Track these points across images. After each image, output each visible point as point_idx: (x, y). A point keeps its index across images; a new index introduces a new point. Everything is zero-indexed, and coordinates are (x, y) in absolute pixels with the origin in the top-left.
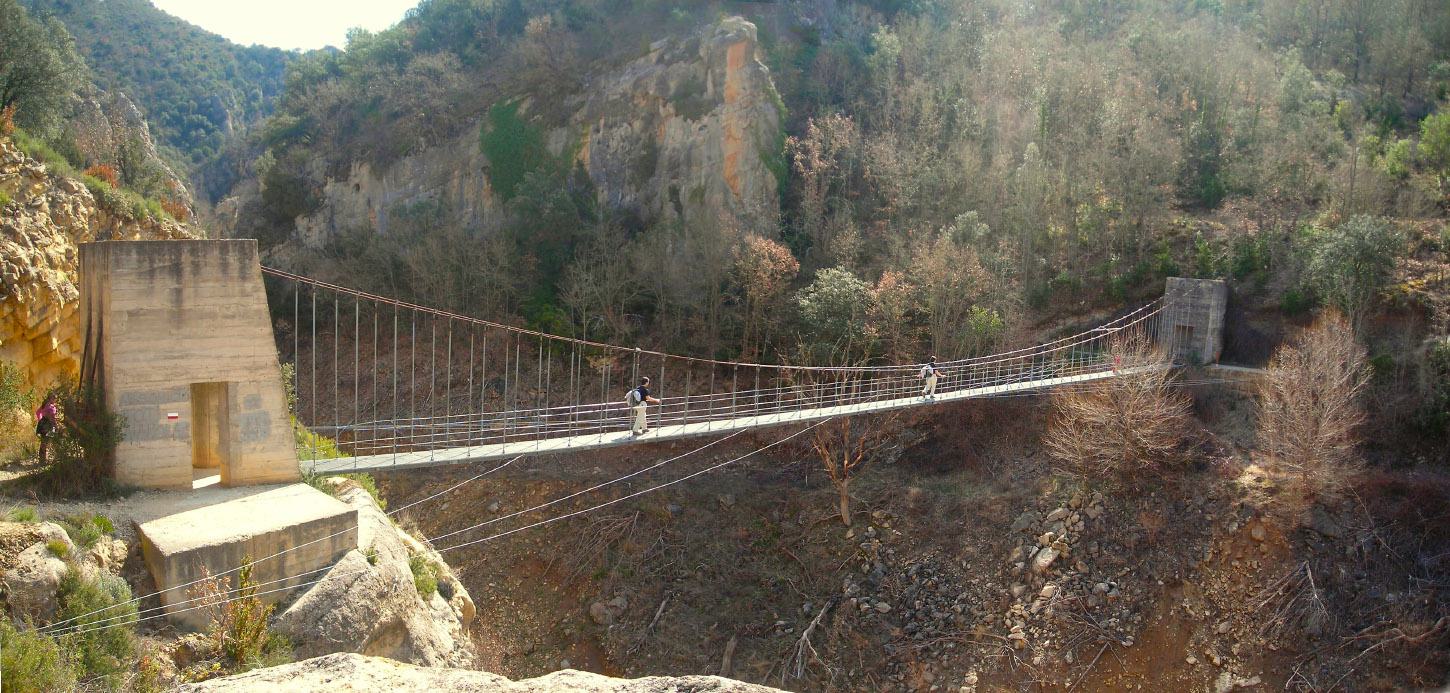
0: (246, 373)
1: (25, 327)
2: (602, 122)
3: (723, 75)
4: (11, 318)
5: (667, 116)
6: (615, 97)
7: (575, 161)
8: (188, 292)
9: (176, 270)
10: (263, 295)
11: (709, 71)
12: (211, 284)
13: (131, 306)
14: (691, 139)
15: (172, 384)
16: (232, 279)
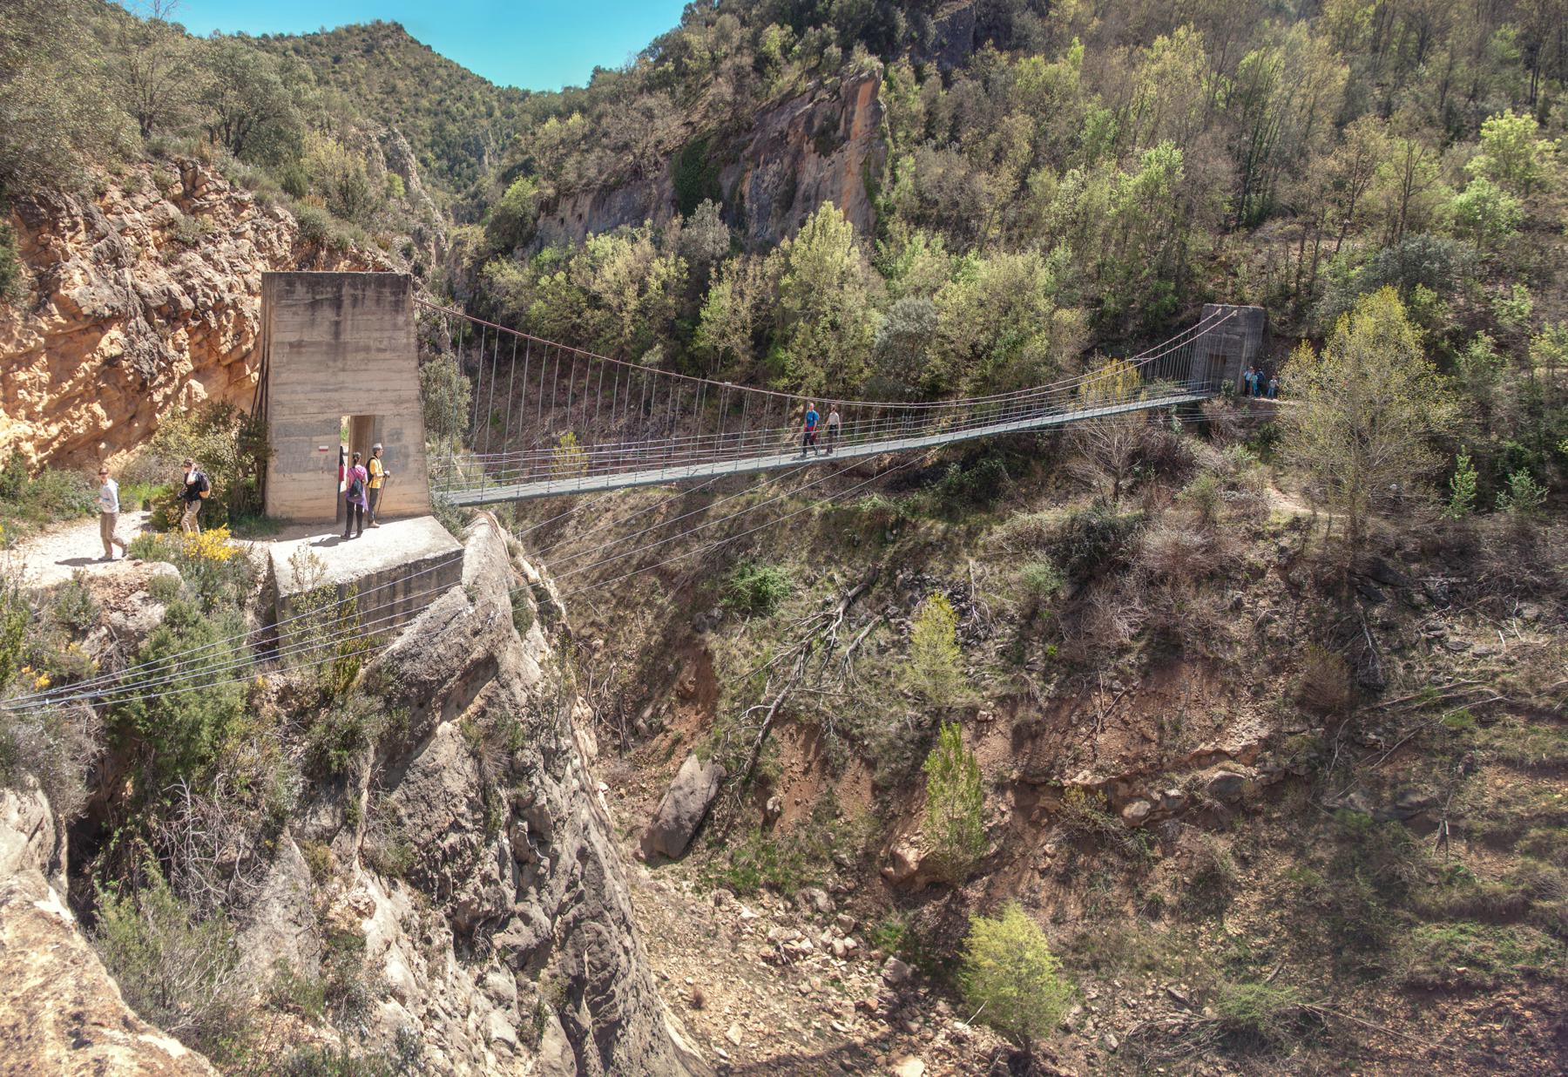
0: (391, 406)
1: (219, 353)
3: (853, 113)
4: (205, 343)
8: (347, 325)
9: (337, 304)
13: (293, 337)
15: (325, 416)
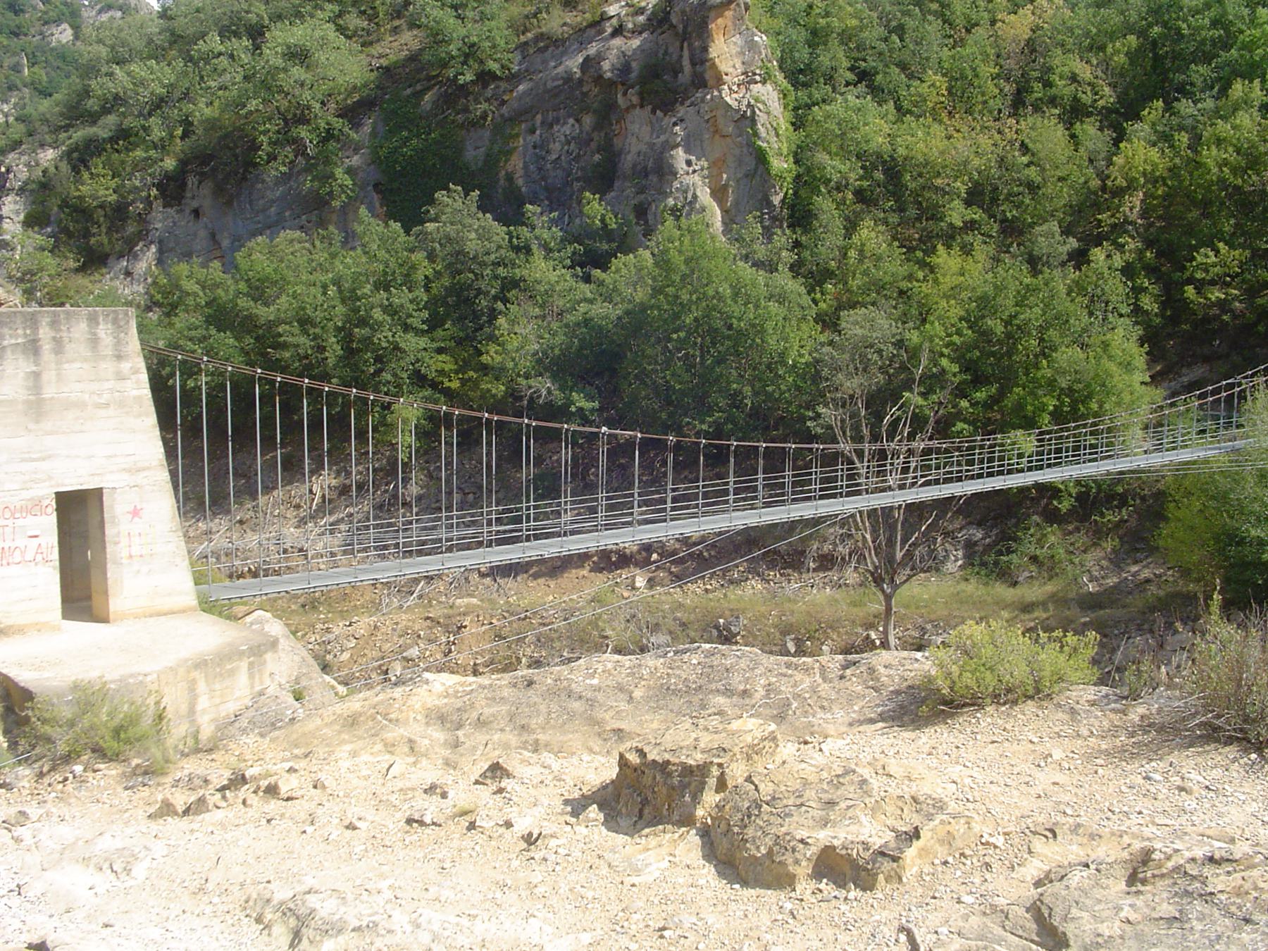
2: (539, 117)
5: (627, 110)
6: (556, 83)
7: (503, 173)
8: (49, 376)
10: (144, 377)
11: (685, 45)
12: (78, 365)
14: (663, 138)
16: (104, 358)
